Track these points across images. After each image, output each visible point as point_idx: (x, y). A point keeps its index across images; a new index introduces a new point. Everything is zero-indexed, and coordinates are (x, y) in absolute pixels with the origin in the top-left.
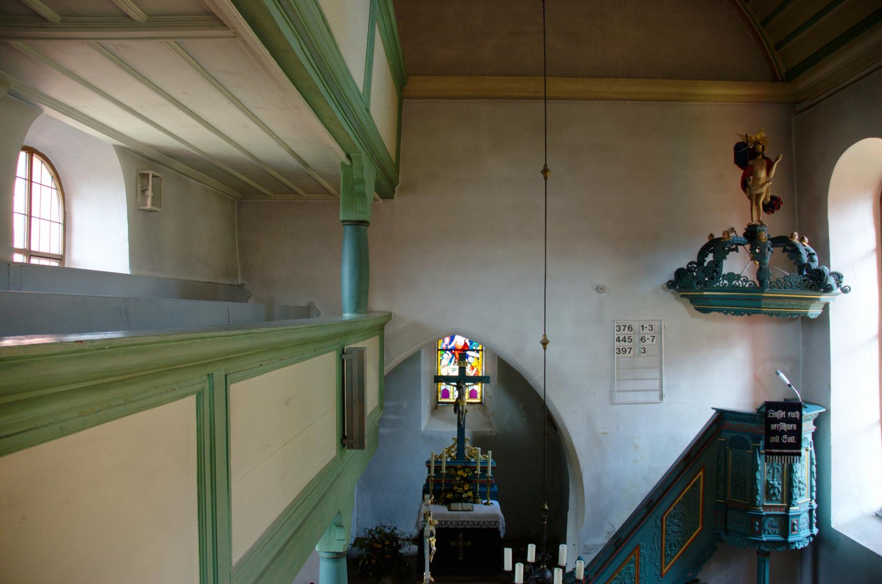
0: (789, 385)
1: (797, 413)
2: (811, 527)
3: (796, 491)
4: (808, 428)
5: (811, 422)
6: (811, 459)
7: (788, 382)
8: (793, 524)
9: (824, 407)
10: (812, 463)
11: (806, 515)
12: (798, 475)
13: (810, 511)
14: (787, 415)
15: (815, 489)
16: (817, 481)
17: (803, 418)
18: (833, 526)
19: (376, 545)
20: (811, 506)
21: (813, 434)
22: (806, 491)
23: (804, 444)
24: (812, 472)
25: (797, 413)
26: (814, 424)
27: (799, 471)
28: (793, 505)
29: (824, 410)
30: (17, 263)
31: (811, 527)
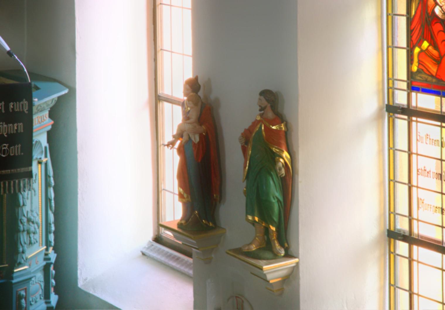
0: (9, 53)
1: (25, 102)
2: (47, 296)
3: (24, 238)
4: (41, 123)
5: (46, 113)
6: (47, 176)
7: (8, 48)
8: (20, 297)
9: (66, 86)
10: (47, 185)
11: (40, 276)
12: (27, 209)
13: (46, 269)
14: (441, 124)
15: (53, 228)
16: (56, 214)
17: (34, 109)
18: (81, 284)
19: (23, 301)
20: (47, 258)
21: (49, 133)
22: (39, 235)
23: (36, 154)
24: (48, 199)
25: (25, 102)
26: (51, 116)
27: (28, 202)
28: (20, 264)
29: (66, 91)
30: (411, 110)
31: (47, 296)
